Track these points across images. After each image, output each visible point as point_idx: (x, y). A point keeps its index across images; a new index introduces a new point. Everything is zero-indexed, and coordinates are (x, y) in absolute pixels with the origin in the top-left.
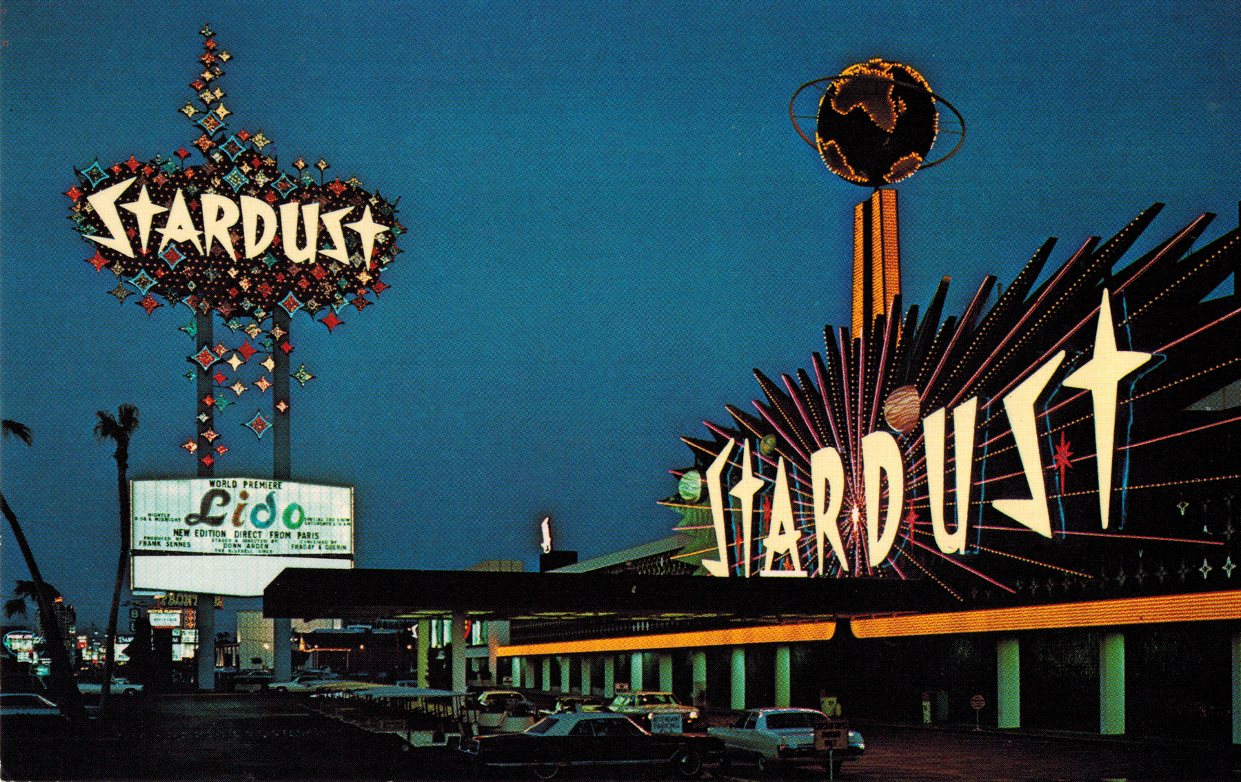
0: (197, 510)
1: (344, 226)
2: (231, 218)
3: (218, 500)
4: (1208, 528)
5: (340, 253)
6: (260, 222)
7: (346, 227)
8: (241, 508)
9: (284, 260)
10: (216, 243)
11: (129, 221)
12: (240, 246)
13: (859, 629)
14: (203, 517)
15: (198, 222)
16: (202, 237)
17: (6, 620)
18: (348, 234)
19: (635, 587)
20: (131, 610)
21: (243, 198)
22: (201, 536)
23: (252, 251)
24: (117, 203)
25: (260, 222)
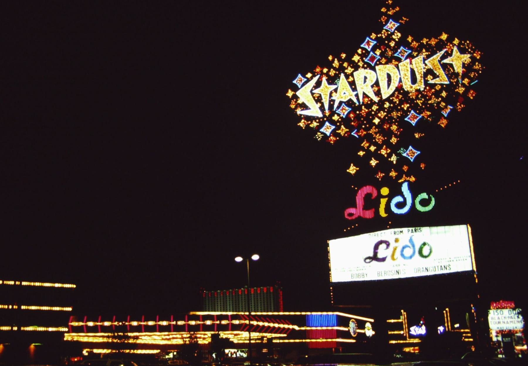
0: (371, 255)
1: (442, 63)
2: (372, 79)
3: (383, 246)
4: (479, 296)
5: (443, 79)
6: (389, 77)
7: (443, 63)
8: (395, 249)
9: (406, 94)
10: (365, 95)
11: (319, 100)
12: (378, 93)
13: (5, 282)
14: (375, 258)
15: (353, 85)
16: (357, 96)
17: (499, 337)
18: (445, 67)
19: (478, 296)
20: (424, 60)
21: (377, 67)
22: (397, 234)
23: (386, 93)
24: (311, 91)
25: (389, 77)
